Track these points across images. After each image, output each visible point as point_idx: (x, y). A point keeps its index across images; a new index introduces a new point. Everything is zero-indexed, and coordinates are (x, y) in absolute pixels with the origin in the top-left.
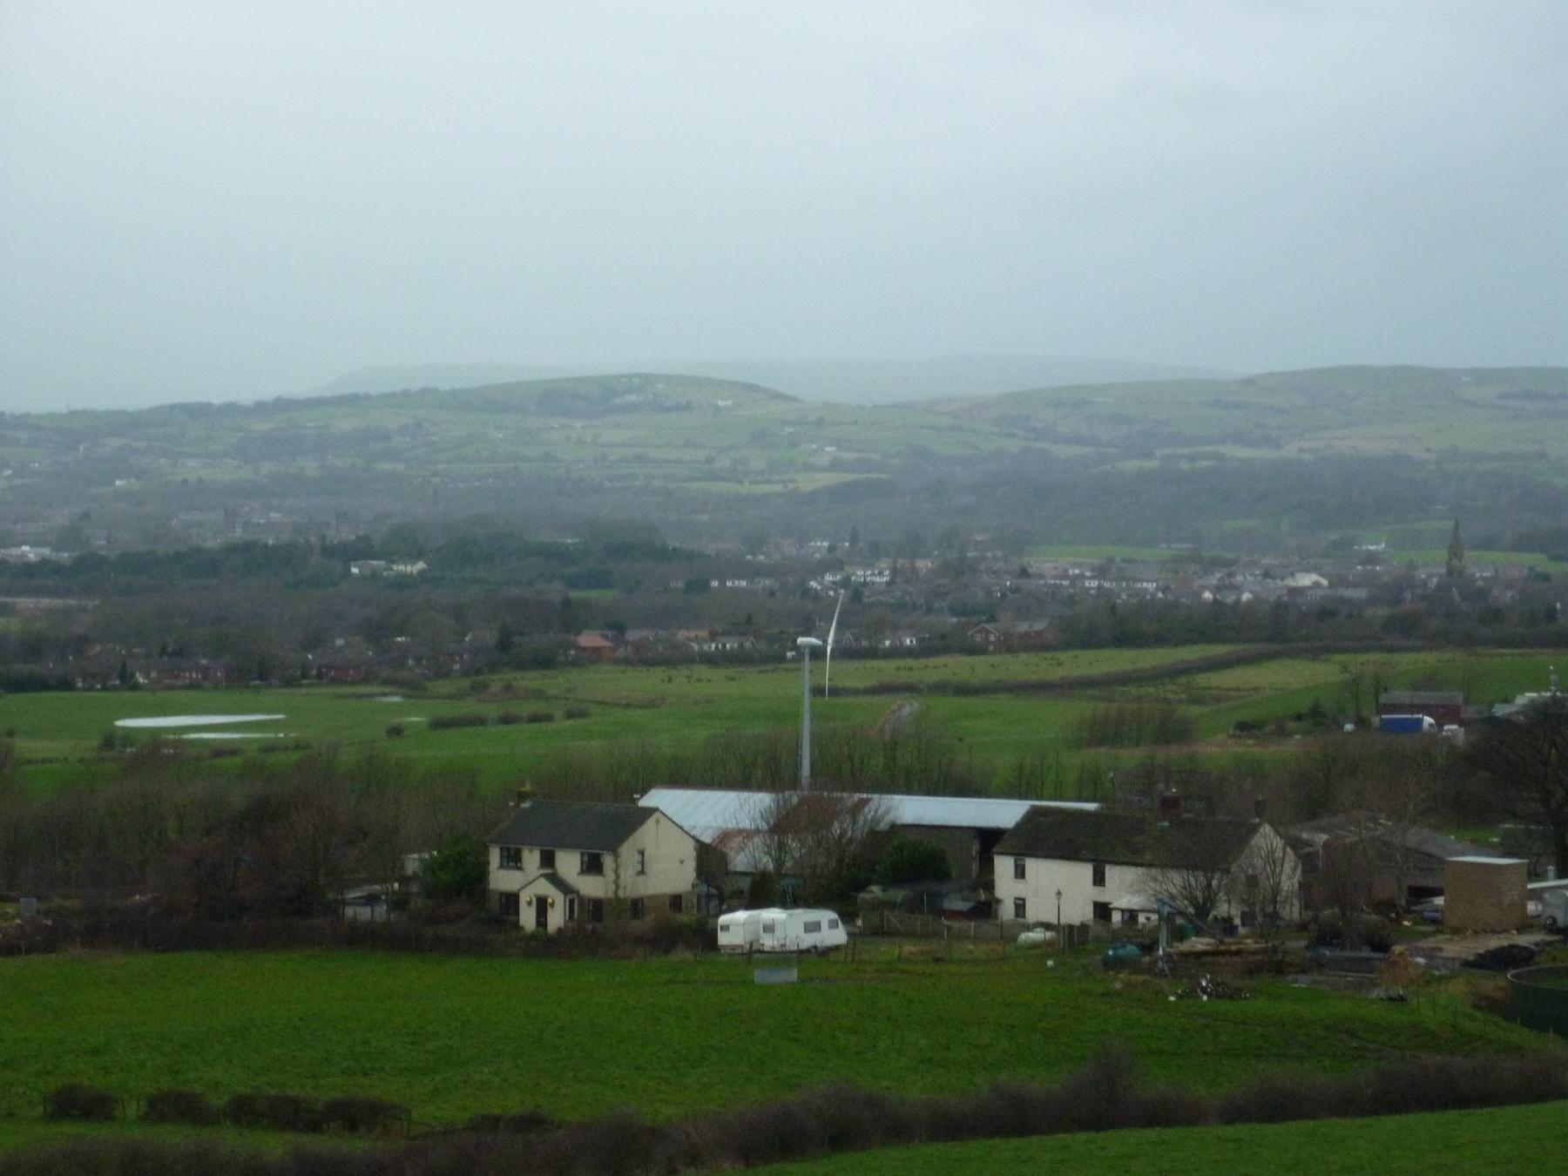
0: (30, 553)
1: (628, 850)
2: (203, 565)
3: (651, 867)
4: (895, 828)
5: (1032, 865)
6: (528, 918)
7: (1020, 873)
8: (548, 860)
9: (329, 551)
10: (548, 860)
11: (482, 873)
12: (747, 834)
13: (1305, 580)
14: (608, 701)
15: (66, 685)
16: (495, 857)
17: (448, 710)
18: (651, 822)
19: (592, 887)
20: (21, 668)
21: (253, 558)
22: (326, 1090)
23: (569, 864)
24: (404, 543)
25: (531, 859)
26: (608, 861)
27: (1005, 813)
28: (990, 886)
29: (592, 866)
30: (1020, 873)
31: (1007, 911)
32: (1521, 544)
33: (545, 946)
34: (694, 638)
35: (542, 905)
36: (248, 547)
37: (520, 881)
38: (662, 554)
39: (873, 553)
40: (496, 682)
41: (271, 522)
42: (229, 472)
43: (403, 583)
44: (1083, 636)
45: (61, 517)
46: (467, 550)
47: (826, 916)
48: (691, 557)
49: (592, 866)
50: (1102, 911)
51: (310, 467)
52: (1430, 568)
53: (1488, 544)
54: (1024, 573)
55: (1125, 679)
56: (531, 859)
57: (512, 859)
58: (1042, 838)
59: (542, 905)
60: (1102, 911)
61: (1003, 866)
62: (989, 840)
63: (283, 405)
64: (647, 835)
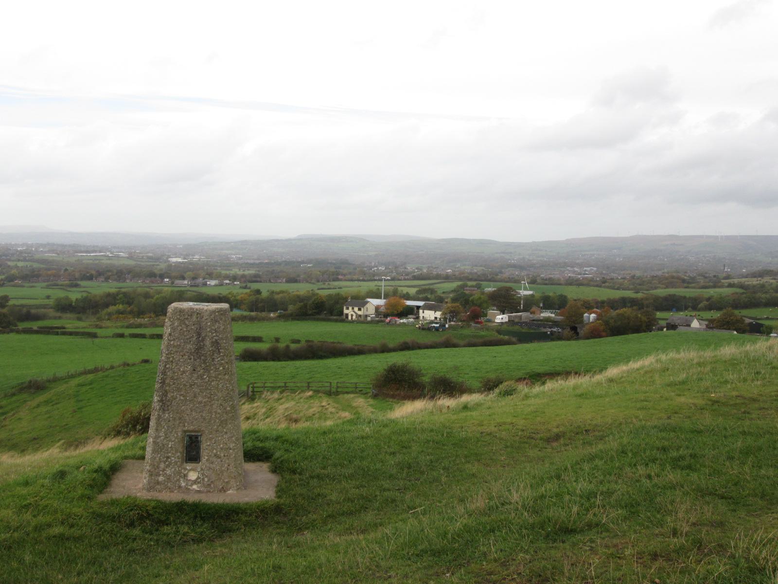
0: (266, 261)
1: (365, 307)
3: (369, 310)
4: (408, 306)
5: (425, 311)
6: (350, 318)
7: (423, 312)
8: (353, 309)
9: (298, 262)
10: (353, 309)
11: (343, 311)
12: (382, 306)
13: (449, 271)
14: (348, 288)
15: (261, 282)
16: (345, 308)
17: (321, 287)
18: (368, 304)
19: (360, 313)
20: (254, 279)
21: (287, 263)
22: (91, 367)
23: (356, 309)
24: (310, 262)
25: (350, 308)
26: (362, 309)
27: (421, 303)
28: (419, 314)
29: (360, 309)
30: (423, 312)
31: (421, 318)
32: (481, 266)
33: (352, 322)
35: (352, 315)
36: (285, 261)
39: (382, 264)
40: (327, 283)
43: (309, 267)
44: (415, 278)
46: (318, 263)
48: (353, 264)
49: (360, 309)
54: (406, 268)
55: (424, 285)
56: (350, 308)
57: (348, 309)
59: (352, 315)
61: (421, 311)
62: (418, 307)
64: (368, 305)
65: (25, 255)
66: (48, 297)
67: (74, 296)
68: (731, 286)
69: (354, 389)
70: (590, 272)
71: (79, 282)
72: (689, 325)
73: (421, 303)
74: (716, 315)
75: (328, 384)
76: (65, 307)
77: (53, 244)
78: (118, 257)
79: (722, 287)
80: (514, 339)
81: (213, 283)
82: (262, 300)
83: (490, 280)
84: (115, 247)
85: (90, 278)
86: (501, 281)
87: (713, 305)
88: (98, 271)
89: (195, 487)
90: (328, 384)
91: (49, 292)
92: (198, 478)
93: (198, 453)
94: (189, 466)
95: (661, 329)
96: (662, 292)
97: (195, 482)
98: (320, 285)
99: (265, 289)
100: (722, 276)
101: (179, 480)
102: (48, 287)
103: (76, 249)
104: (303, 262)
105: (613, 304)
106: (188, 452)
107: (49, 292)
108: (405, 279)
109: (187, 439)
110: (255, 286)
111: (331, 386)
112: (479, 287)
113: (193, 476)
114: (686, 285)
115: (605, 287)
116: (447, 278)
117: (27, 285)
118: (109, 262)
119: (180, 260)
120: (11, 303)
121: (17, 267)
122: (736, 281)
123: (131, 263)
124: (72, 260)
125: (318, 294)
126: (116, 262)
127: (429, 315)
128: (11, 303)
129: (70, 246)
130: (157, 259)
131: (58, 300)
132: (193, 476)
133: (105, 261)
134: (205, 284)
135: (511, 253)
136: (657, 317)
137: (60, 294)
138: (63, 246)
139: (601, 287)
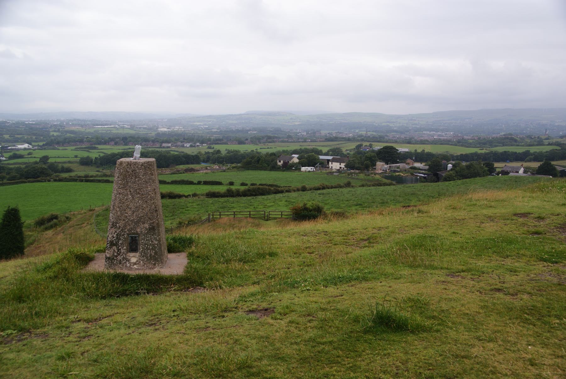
2: (232, 131)
21: (238, 131)
24: (255, 129)
27: (330, 158)
32: (373, 132)
34: (300, 140)
37: (496, 165)
38: (282, 131)
41: (240, 127)
42: (235, 122)
43: (254, 134)
45: (217, 126)
47: (313, 168)
50: (341, 168)
51: (243, 121)
52: (364, 133)
53: (369, 131)
58: (334, 160)
60: (341, 168)
61: (330, 163)
62: (328, 161)
63: (240, 114)
65: (59, 127)
66: (76, 157)
67: (94, 155)
68: (549, 144)
69: (280, 216)
70: (449, 135)
71: (97, 146)
72: (518, 172)
73: (330, 158)
74: (536, 165)
75: (263, 212)
76: (86, 162)
77: (79, 120)
78: (123, 128)
79: (543, 145)
80: (394, 183)
81: (188, 145)
82: (221, 158)
83: (379, 142)
84: (121, 122)
85: (105, 143)
86: (387, 142)
87: (536, 157)
88: (110, 138)
89: (135, 266)
90: (263, 212)
91: (76, 153)
92: (137, 261)
93: (137, 247)
94: (132, 254)
95: (498, 174)
96: (500, 149)
97: (135, 264)
98: (261, 146)
99: (223, 149)
100: (543, 137)
101: (126, 263)
102: (76, 149)
103: (95, 123)
104: (250, 130)
105: (464, 157)
106: (131, 247)
107: (76, 153)
108: (320, 141)
109: (130, 238)
110: (217, 147)
111: (265, 214)
112: (371, 146)
113: (134, 260)
114: (461, 144)
115: (459, 146)
116: (349, 140)
117: (60, 148)
118: (116, 132)
119: (166, 130)
120: (50, 161)
121: (53, 135)
122: (554, 141)
123: (132, 132)
124: (92, 130)
125: (260, 153)
126: (121, 131)
127: (335, 166)
128: (50, 161)
129: (90, 121)
130: (150, 129)
131: (82, 159)
132: (134, 260)
133: (114, 131)
134: (183, 146)
135: (394, 122)
136: (495, 166)
137: (85, 154)
138: (84, 121)
139: (456, 145)
